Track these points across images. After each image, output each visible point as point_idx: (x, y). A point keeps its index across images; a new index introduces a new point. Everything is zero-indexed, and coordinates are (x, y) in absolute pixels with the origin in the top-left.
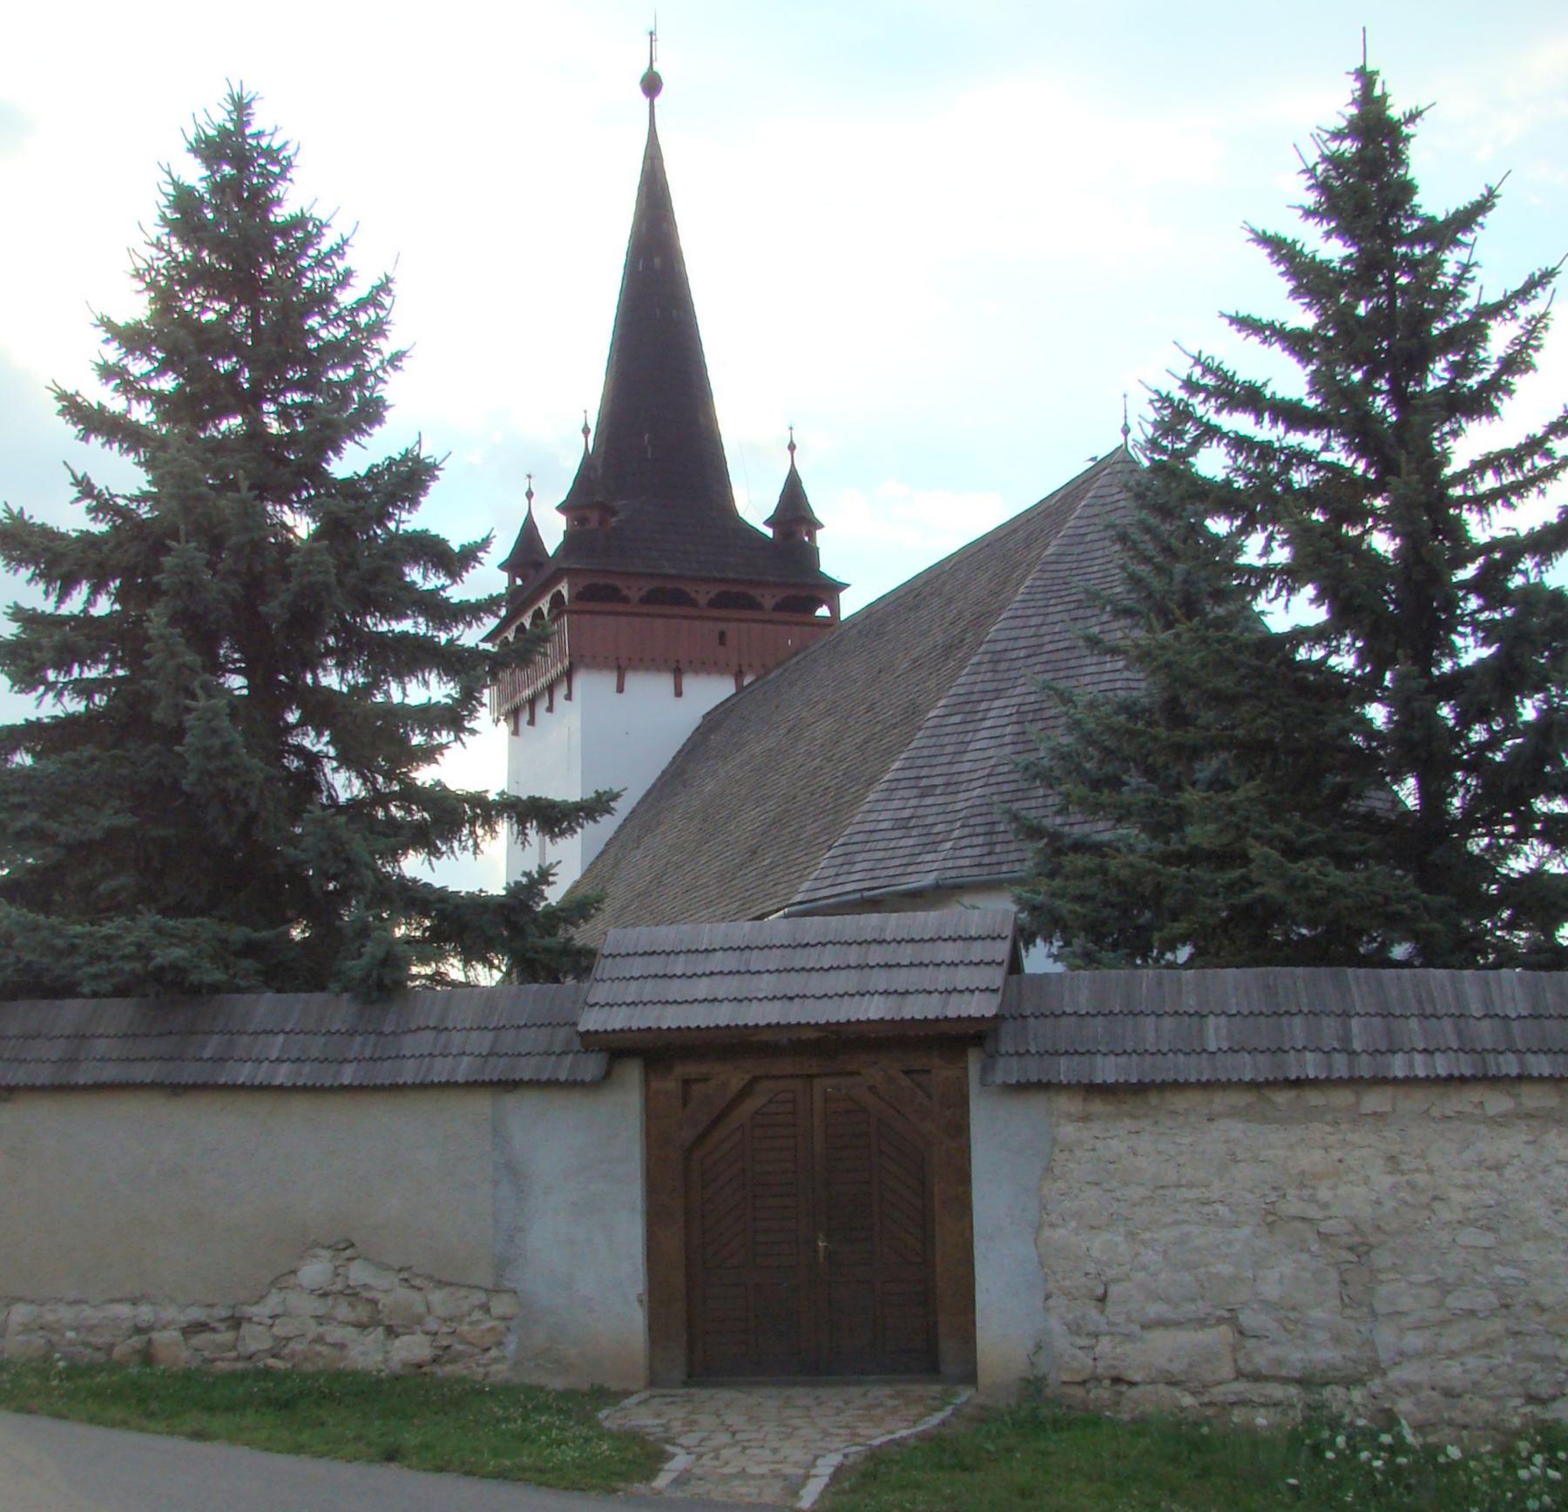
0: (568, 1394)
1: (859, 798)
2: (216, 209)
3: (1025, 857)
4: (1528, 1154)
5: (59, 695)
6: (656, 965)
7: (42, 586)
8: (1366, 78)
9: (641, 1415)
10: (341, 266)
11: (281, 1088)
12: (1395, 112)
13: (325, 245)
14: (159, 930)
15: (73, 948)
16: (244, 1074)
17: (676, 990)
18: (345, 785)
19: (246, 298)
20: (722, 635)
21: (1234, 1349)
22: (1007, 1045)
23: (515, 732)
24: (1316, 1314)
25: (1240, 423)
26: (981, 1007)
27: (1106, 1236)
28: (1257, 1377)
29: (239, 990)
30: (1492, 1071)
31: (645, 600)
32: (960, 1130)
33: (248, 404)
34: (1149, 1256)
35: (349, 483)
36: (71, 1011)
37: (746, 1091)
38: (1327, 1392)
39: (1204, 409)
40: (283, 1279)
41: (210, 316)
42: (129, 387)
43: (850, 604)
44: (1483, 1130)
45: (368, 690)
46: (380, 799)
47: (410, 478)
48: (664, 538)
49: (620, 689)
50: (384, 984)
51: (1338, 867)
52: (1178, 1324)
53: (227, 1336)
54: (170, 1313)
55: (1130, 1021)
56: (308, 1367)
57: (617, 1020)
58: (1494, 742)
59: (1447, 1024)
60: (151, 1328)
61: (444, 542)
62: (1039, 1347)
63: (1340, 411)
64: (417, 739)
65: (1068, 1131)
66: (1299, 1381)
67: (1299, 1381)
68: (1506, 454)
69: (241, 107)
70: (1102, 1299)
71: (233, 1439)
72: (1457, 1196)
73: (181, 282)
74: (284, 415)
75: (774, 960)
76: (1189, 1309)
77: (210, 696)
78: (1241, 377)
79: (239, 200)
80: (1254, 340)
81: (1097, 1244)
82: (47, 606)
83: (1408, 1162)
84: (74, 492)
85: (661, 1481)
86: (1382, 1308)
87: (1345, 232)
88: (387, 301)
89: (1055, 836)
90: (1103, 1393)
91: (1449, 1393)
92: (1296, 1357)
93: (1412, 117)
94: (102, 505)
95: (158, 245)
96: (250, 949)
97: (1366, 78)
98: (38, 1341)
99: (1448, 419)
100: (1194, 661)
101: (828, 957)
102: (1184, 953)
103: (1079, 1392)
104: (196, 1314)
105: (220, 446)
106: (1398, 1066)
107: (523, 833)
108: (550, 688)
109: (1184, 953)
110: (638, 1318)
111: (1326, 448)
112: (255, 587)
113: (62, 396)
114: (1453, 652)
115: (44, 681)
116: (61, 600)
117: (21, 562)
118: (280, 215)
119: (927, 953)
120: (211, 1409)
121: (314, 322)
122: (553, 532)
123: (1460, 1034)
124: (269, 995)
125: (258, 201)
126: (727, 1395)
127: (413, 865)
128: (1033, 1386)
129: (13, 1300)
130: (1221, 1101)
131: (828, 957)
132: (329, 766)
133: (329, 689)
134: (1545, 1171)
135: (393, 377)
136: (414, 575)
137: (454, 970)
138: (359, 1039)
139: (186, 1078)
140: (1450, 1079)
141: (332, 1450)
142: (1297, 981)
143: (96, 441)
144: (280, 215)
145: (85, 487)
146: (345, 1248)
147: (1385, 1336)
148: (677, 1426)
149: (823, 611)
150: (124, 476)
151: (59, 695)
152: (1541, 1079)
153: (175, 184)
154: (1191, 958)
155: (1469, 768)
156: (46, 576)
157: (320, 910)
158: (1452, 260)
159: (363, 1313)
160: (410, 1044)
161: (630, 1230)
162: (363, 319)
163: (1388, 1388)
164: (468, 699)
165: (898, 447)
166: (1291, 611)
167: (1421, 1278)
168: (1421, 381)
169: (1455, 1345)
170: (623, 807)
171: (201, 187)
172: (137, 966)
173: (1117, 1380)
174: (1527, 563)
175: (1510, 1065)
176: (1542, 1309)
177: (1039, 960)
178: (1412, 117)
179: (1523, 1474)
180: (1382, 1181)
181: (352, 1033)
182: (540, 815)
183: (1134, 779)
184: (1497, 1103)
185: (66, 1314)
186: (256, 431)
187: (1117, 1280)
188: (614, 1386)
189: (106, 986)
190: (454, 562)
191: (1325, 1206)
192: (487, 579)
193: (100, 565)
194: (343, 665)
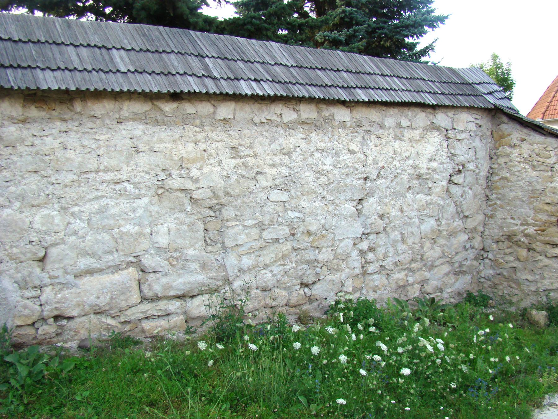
4: (303, 144)
24: (191, 252)
28: (156, 298)
52: (100, 271)
70: (42, 260)
81: (38, 219)
86: (229, 243)
103: (31, 331)
134: (312, 155)
167: (250, 223)
176: (309, 233)
184: (288, 114)
191: (197, 180)
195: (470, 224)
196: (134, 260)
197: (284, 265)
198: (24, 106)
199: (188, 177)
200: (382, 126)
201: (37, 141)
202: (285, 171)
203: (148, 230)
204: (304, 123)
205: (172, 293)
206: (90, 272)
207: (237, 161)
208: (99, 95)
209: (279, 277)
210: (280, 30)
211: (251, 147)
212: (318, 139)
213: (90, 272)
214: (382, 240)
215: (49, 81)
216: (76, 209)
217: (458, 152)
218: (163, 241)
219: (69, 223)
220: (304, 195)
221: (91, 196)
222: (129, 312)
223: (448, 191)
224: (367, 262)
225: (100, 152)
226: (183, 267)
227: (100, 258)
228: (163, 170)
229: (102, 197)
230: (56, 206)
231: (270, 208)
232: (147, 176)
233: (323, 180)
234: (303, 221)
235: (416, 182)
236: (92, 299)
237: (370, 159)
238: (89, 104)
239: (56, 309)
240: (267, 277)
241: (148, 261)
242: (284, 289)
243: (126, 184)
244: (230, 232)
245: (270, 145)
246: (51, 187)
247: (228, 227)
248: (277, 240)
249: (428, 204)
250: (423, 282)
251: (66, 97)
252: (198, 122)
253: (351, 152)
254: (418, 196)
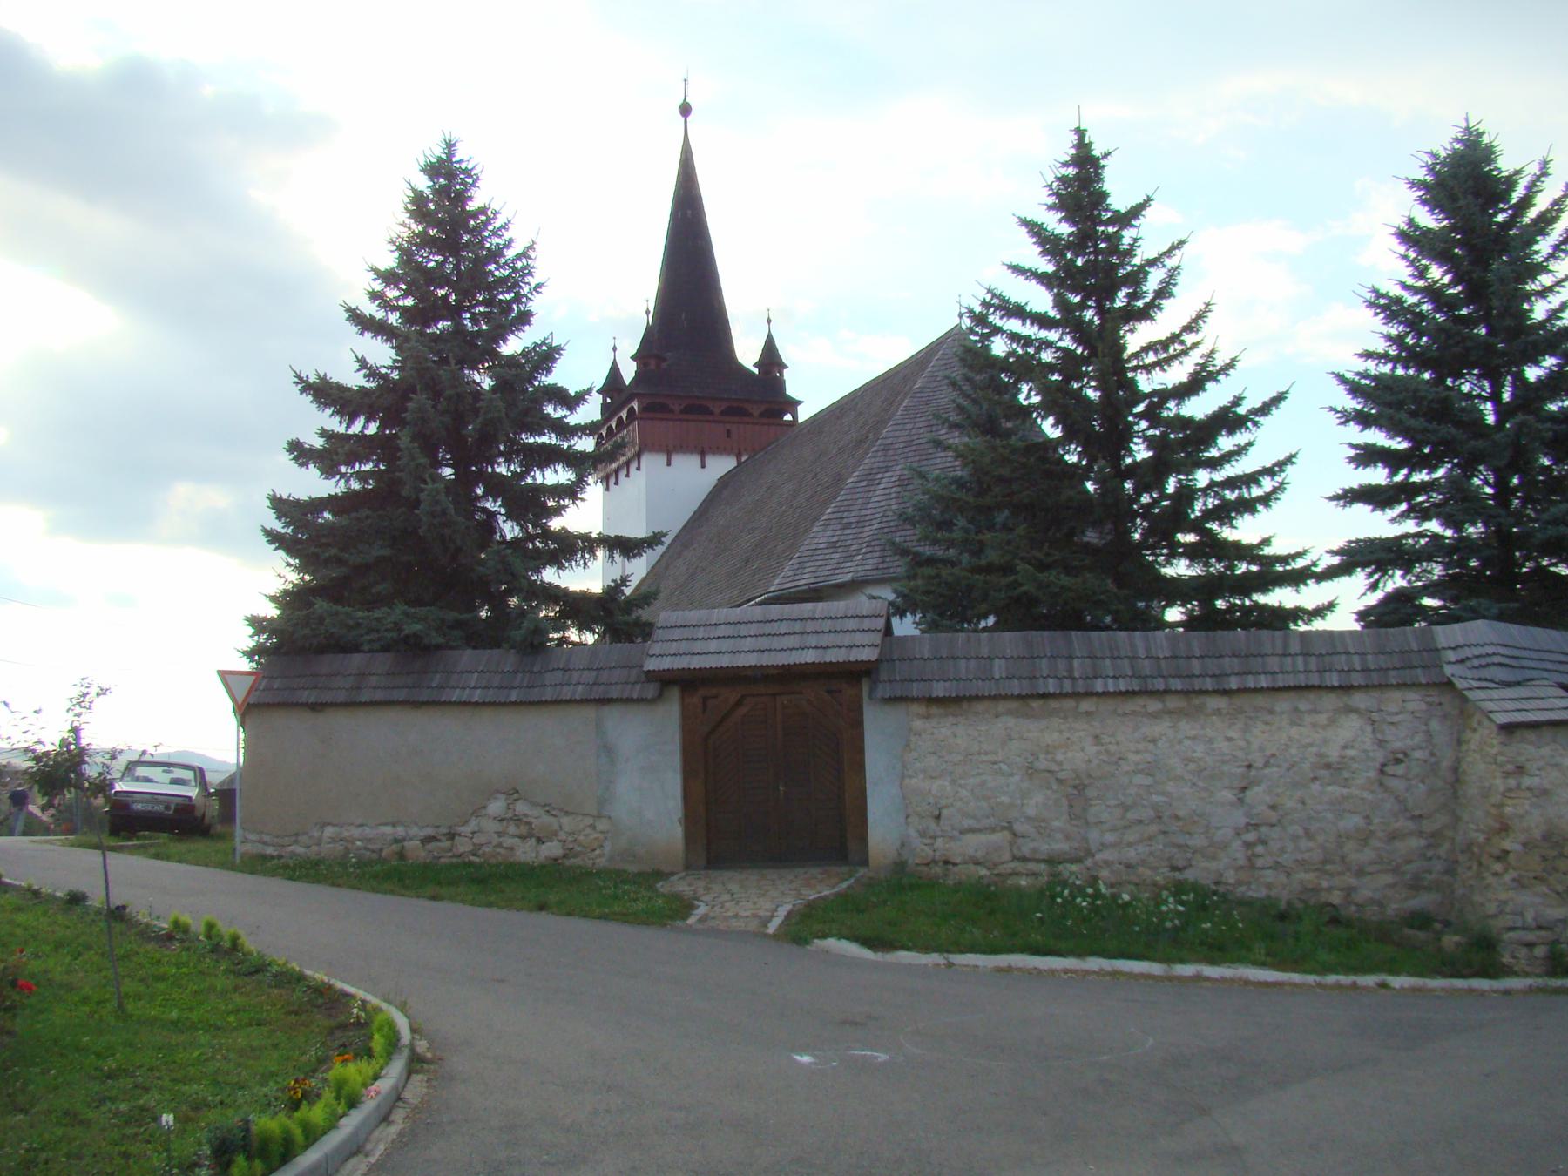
0: (640, 874)
1: (807, 531)
2: (436, 203)
3: (898, 566)
4: (1170, 733)
5: (347, 481)
6: (687, 633)
7: (338, 419)
8: (1080, 133)
9: (682, 885)
10: (507, 235)
11: (477, 704)
12: (1096, 152)
13: (498, 224)
14: (407, 615)
15: (359, 625)
16: (456, 696)
17: (698, 647)
18: (510, 530)
19: (454, 266)
20: (729, 432)
21: (1011, 844)
22: (883, 676)
23: (607, 489)
24: (1056, 824)
25: (1014, 325)
26: (868, 655)
27: (939, 782)
28: (1024, 859)
29: (452, 648)
30: (1150, 687)
31: (682, 412)
32: (858, 724)
33: (454, 313)
34: (964, 793)
35: (512, 357)
36: (356, 660)
37: (739, 703)
38: (1061, 867)
39: (995, 319)
40: (478, 811)
41: (432, 264)
42: (387, 305)
43: (804, 414)
44: (1145, 720)
45: (522, 476)
46: (531, 538)
47: (546, 356)
48: (692, 373)
49: (669, 464)
50: (534, 645)
51: (1068, 574)
52: (979, 831)
53: (448, 844)
54: (414, 830)
55: (951, 662)
56: (493, 861)
57: (666, 664)
58: (1155, 502)
59: (1126, 662)
60: (404, 840)
61: (566, 391)
62: (903, 845)
63: (1068, 319)
64: (551, 503)
65: (918, 724)
66: (1044, 861)
67: (1044, 861)
68: (1159, 342)
69: (450, 145)
70: (938, 817)
71: (452, 899)
72: (1133, 757)
73: (416, 245)
74: (474, 320)
75: (753, 629)
76: (986, 823)
77: (434, 481)
78: (1013, 300)
79: (449, 198)
80: (1021, 278)
81: (935, 786)
82: (342, 430)
83: (1106, 739)
84: (357, 366)
85: (691, 920)
86: (1091, 819)
87: (1068, 219)
88: (531, 253)
89: (917, 554)
90: (938, 870)
91: (1129, 866)
92: (1045, 848)
93: (1106, 155)
94: (373, 373)
95: (404, 225)
96: (459, 624)
97: (1080, 133)
98: (340, 847)
99: (1127, 322)
100: (987, 460)
101: (784, 628)
102: (991, 620)
103: (926, 869)
104: (430, 831)
105: (436, 338)
106: (1099, 686)
107: (611, 556)
108: (628, 464)
109: (991, 620)
110: (678, 831)
111: (1061, 339)
112: (460, 419)
113: (349, 310)
114: (1130, 453)
115: (339, 472)
116: (348, 426)
117: (326, 405)
118: (472, 206)
119: (839, 625)
120: (439, 883)
121: (492, 267)
122: (629, 372)
123: (1132, 667)
124: (469, 651)
125: (461, 198)
126: (728, 874)
127: (549, 575)
128: (900, 866)
129: (324, 825)
130: (1002, 706)
131: (784, 628)
132: (501, 519)
133: (500, 474)
134: (1180, 742)
135: (536, 297)
136: (549, 409)
137: (573, 635)
138: (520, 676)
139: (424, 698)
140: (1127, 692)
141: (509, 904)
142: (1043, 639)
143: (368, 335)
144: (472, 206)
145: (363, 363)
146: (513, 793)
147: (1094, 835)
148: (701, 891)
149: (788, 417)
150: (382, 354)
151: (347, 481)
152: (1177, 692)
153: (413, 190)
154: (996, 623)
155: (1143, 517)
156: (340, 412)
157: (497, 602)
158: (1127, 236)
159: (524, 830)
160: (549, 678)
161: (673, 782)
162: (519, 265)
163: (1096, 864)
164: (580, 483)
165: (834, 322)
166: (1050, 428)
167: (1113, 802)
168: (1113, 301)
169: (1131, 839)
170: (667, 540)
171: (428, 192)
172: (395, 635)
173: (946, 862)
174: (1171, 404)
175: (1159, 684)
176: (1177, 818)
177: (905, 627)
178: (1106, 155)
179: (1164, 908)
180: (1092, 750)
181: (516, 672)
182: (624, 546)
183: (961, 522)
184: (1154, 705)
185: (356, 832)
186: (459, 329)
187: (946, 807)
188: (665, 869)
189: (376, 646)
190: (571, 401)
191: (1060, 764)
192: (590, 412)
193: (371, 406)
194: (509, 461)
195: (1428, 826)
200: (1271, 712)
206: (972, 830)
210: (1051, 420)
212: (1186, 727)
214: (1275, 833)
217: (1388, 738)
223: (1381, 784)
224: (1254, 855)
231: (1132, 791)
233: (1192, 766)
235: (1323, 772)
236: (971, 852)
237: (1255, 746)
240: (1131, 854)
241: (1018, 827)
248: (1141, 822)
249: (1345, 798)
250: (1349, 891)
253: (1229, 739)
254: (1330, 788)
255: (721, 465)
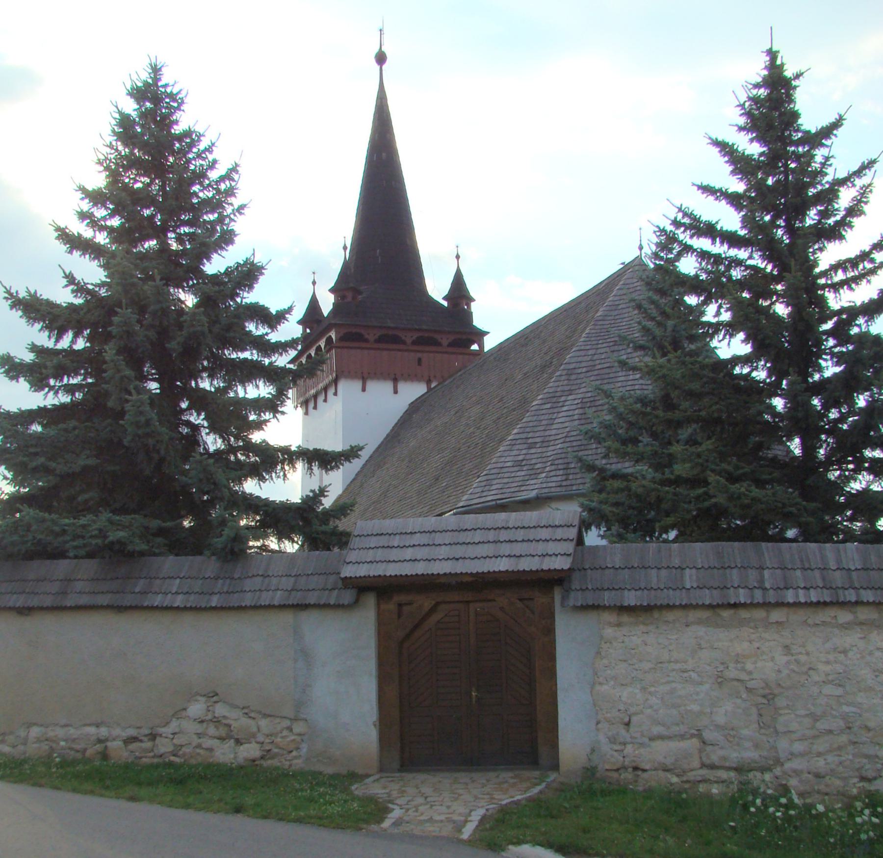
4: (861, 644)
23: (306, 413)
24: (745, 732)
28: (713, 767)
52: (670, 738)
70: (628, 724)
86: (780, 728)
176: (868, 729)
184: (844, 616)
191: (750, 673)
196: (696, 732)
197: (840, 756)
198: (618, 615)
199: (743, 669)
201: (626, 639)
202: (839, 668)
203: (709, 710)
204: (861, 624)
205: (727, 764)
206: (661, 737)
207: (789, 658)
208: (669, 607)
209: (833, 766)
211: (804, 646)
213: (661, 737)
215: (631, 598)
216: (652, 689)
218: (721, 719)
219: (647, 699)
220: (860, 691)
221: (664, 681)
222: (689, 774)
225: (671, 648)
226: (738, 744)
227: (668, 728)
228: (722, 663)
229: (673, 682)
230: (638, 686)
232: (708, 668)
234: (860, 716)
238: (664, 612)
239: (634, 761)
240: (820, 764)
241: (708, 735)
242: (839, 778)
243: (691, 673)
244: (781, 719)
245: (823, 644)
246: (635, 672)
247: (781, 715)
248: (830, 732)
251: (648, 609)
252: (752, 624)
255: (413, 391)
